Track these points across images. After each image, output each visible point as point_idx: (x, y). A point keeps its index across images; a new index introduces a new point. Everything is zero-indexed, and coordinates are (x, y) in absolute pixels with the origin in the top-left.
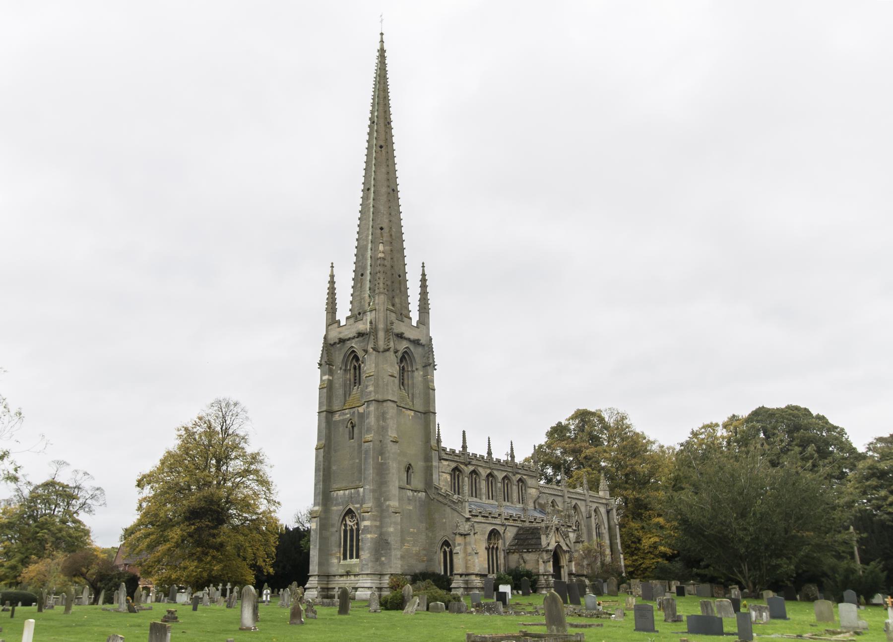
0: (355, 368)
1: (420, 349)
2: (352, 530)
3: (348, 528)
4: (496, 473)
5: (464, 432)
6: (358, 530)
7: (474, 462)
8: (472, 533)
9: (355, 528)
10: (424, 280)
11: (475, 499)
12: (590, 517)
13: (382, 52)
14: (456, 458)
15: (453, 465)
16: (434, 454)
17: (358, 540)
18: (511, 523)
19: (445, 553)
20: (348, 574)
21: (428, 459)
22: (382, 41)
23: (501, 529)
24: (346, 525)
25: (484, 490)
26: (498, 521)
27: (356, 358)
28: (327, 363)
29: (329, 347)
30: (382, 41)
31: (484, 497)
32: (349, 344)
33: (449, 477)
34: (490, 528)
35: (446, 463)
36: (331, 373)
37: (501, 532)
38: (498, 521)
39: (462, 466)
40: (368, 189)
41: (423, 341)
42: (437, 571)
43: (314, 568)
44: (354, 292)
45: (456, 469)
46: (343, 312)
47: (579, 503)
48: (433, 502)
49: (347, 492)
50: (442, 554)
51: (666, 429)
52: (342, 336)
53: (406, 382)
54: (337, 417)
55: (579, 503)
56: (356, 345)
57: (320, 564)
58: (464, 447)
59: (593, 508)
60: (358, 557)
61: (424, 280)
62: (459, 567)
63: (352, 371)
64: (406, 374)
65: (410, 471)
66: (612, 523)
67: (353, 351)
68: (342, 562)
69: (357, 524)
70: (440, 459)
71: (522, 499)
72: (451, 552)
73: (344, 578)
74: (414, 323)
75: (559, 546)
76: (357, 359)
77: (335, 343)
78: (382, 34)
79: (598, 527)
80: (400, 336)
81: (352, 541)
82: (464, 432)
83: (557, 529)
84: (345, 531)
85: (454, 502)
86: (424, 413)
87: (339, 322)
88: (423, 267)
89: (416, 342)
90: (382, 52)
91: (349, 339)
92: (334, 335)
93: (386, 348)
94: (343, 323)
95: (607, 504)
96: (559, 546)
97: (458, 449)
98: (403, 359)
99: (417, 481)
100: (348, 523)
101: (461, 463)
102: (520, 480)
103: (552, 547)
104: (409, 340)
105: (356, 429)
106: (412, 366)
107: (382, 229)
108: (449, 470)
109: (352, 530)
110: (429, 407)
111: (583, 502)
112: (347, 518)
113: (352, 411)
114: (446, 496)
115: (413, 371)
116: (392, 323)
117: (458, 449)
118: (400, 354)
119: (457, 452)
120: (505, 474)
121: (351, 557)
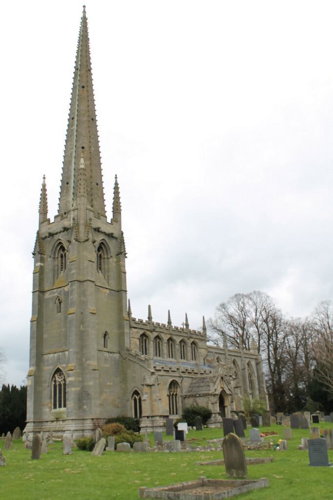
0: (62, 257)
2: (60, 385)
3: (57, 383)
4: (174, 337)
6: (65, 385)
7: (157, 329)
10: (116, 188)
13: (84, 20)
15: (142, 332)
16: (126, 324)
17: (65, 393)
18: (187, 375)
19: (135, 400)
20: (57, 420)
21: (121, 327)
22: (84, 12)
23: (178, 380)
24: (55, 381)
26: (176, 374)
27: (63, 248)
28: (39, 252)
29: (41, 240)
31: (166, 356)
32: (56, 237)
33: (138, 342)
34: (171, 380)
35: (135, 330)
36: (42, 260)
37: (179, 382)
42: (129, 415)
43: (30, 416)
45: (144, 335)
46: (53, 211)
49: (56, 355)
50: (133, 402)
52: (51, 231)
53: (103, 267)
54: (47, 295)
56: (62, 237)
57: (35, 413)
60: (65, 406)
61: (116, 188)
62: (146, 411)
63: (60, 259)
64: (102, 260)
65: (107, 337)
67: (60, 243)
68: (53, 410)
69: (64, 380)
70: (131, 327)
72: (140, 399)
73: (55, 423)
74: (109, 221)
75: (223, 391)
78: (84, 7)
79: (250, 376)
80: (97, 230)
81: (60, 393)
83: (222, 378)
84: (55, 386)
85: (142, 360)
87: (49, 220)
88: (116, 178)
89: (111, 236)
90: (84, 20)
91: (56, 234)
92: (45, 231)
94: (52, 220)
95: (256, 359)
96: (223, 391)
97: (145, 319)
98: (100, 249)
99: (112, 345)
100: (57, 379)
101: (148, 330)
102: (193, 343)
103: (218, 392)
104: (105, 233)
105: (62, 305)
106: (107, 255)
108: (138, 336)
109: (60, 385)
111: (239, 358)
112: (56, 376)
115: (108, 258)
116: (91, 220)
117: (145, 319)
118: (97, 244)
119: (144, 321)
121: (60, 406)
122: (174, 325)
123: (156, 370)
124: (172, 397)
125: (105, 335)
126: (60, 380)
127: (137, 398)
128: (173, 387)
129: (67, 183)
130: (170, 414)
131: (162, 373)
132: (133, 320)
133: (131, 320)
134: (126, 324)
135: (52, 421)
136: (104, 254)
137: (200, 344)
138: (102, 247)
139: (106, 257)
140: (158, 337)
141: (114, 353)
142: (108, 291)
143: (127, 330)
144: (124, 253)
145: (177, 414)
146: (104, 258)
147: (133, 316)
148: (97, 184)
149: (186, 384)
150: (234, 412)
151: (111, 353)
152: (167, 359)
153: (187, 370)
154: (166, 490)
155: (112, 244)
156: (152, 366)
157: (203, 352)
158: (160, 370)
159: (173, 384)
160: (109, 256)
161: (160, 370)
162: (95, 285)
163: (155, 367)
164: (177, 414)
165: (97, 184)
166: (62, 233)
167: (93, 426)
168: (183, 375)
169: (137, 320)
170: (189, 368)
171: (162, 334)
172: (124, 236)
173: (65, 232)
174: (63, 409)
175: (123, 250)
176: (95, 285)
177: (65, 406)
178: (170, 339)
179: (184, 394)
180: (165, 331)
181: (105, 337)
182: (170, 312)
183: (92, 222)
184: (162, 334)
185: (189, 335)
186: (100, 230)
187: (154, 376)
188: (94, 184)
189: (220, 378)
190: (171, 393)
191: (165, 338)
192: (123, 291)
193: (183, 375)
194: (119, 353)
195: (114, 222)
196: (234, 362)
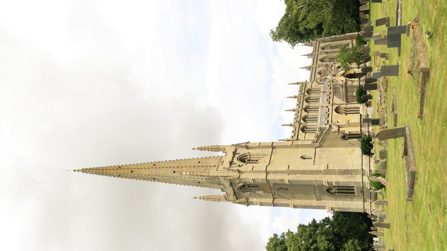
0: (249, 187)
1: (238, 151)
2: (338, 189)
3: (337, 191)
4: (304, 106)
5: (283, 125)
6: (337, 187)
7: (299, 119)
8: (338, 124)
9: (337, 188)
10: (201, 149)
11: (319, 119)
12: (326, 52)
13: (85, 171)
14: (297, 129)
16: (296, 143)
18: (331, 100)
21: (297, 146)
22: (78, 171)
23: (335, 107)
24: (335, 192)
25: (314, 114)
26: (330, 108)
27: (243, 186)
30: (78, 171)
31: (317, 113)
32: (236, 190)
34: (334, 112)
37: (336, 106)
38: (330, 108)
39: (301, 126)
40: (154, 179)
41: (233, 150)
42: (374, 32)
44: (208, 187)
45: (303, 130)
46: (218, 192)
47: (319, 59)
48: (322, 139)
49: (317, 192)
51: (277, 26)
53: (256, 159)
55: (319, 59)
58: (295, 97)
59: (322, 50)
61: (201, 149)
62: (356, 130)
63: (250, 188)
64: (252, 159)
65: (305, 157)
66: (330, 40)
67: (240, 188)
68: (356, 194)
69: (334, 187)
70: (298, 139)
71: (318, 91)
73: (365, 194)
74: (224, 154)
75: (343, 75)
76: (245, 185)
77: (236, 197)
78: (75, 171)
79: (332, 47)
80: (231, 163)
81: (344, 190)
82: (283, 125)
83: (334, 76)
84: (339, 193)
85: (321, 134)
86: (273, 149)
89: (234, 153)
90: (85, 171)
91: (234, 190)
92: (232, 197)
93: (237, 172)
95: (319, 43)
96: (343, 75)
97: (292, 129)
98: (243, 161)
100: (334, 191)
101: (299, 126)
102: (308, 92)
103: (344, 79)
104: (233, 157)
106: (247, 155)
107: (174, 172)
109: (338, 189)
110: (269, 146)
111: (319, 56)
112: (331, 192)
113: (272, 189)
114: (318, 137)
115: (250, 155)
116: (224, 168)
117: (292, 129)
118: (241, 163)
119: (293, 129)
120: (305, 102)
121: (353, 190)
122: (295, 107)
123: (328, 123)
124: (347, 112)
125: (303, 158)
126: (335, 190)
127: (347, 136)
128: (339, 111)
129: (199, 182)
130: (359, 113)
131: (330, 119)
132: (293, 137)
133: (292, 139)
134: (296, 143)
135: (364, 195)
136: (248, 158)
137: (308, 87)
138: (243, 159)
139: (249, 157)
140: (304, 119)
141: (316, 152)
142: (273, 156)
143: (299, 143)
144: (247, 144)
145: (359, 108)
146: (250, 158)
147: (289, 137)
148: (199, 162)
149: (338, 101)
150: (358, 66)
151: (315, 154)
152: (319, 113)
153: (328, 100)
154: (425, 142)
155: (242, 151)
156: (325, 126)
157: (315, 85)
158: (328, 120)
159: (337, 110)
160: (249, 154)
161: (328, 120)
162: (269, 165)
163: (326, 125)
164: (359, 108)
165: (199, 162)
166: (234, 186)
167: (362, 142)
168: (331, 103)
169: (292, 135)
170: (325, 99)
171: (302, 116)
172: (234, 144)
173: (233, 184)
174: (355, 188)
175: (244, 145)
176: (269, 165)
177: (353, 187)
178: (306, 110)
179: (344, 103)
180: (300, 114)
181: (305, 158)
182: (287, 109)
183: (226, 167)
184: (302, 116)
185: (302, 95)
186: (231, 161)
187: (332, 126)
188: (199, 164)
189: (334, 77)
190: (344, 112)
191: (304, 114)
192: (267, 170)
193: (331, 103)
194: (316, 148)
195: (225, 151)
196: (322, 60)
